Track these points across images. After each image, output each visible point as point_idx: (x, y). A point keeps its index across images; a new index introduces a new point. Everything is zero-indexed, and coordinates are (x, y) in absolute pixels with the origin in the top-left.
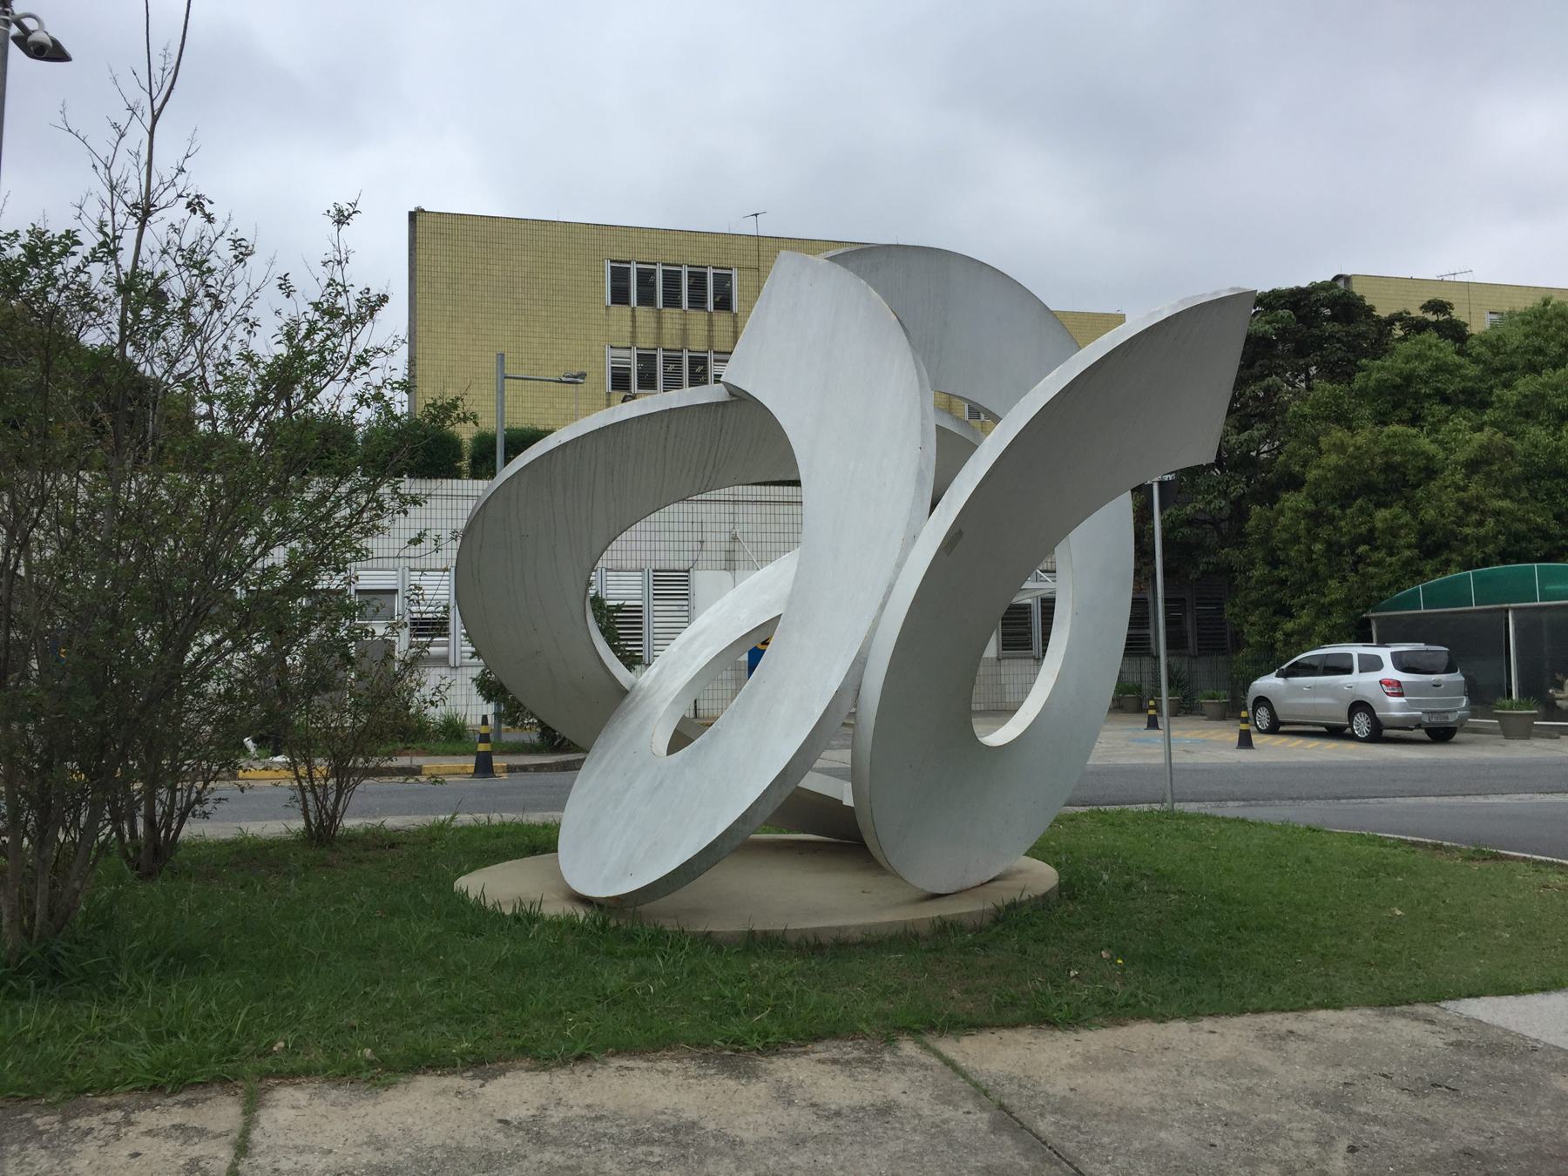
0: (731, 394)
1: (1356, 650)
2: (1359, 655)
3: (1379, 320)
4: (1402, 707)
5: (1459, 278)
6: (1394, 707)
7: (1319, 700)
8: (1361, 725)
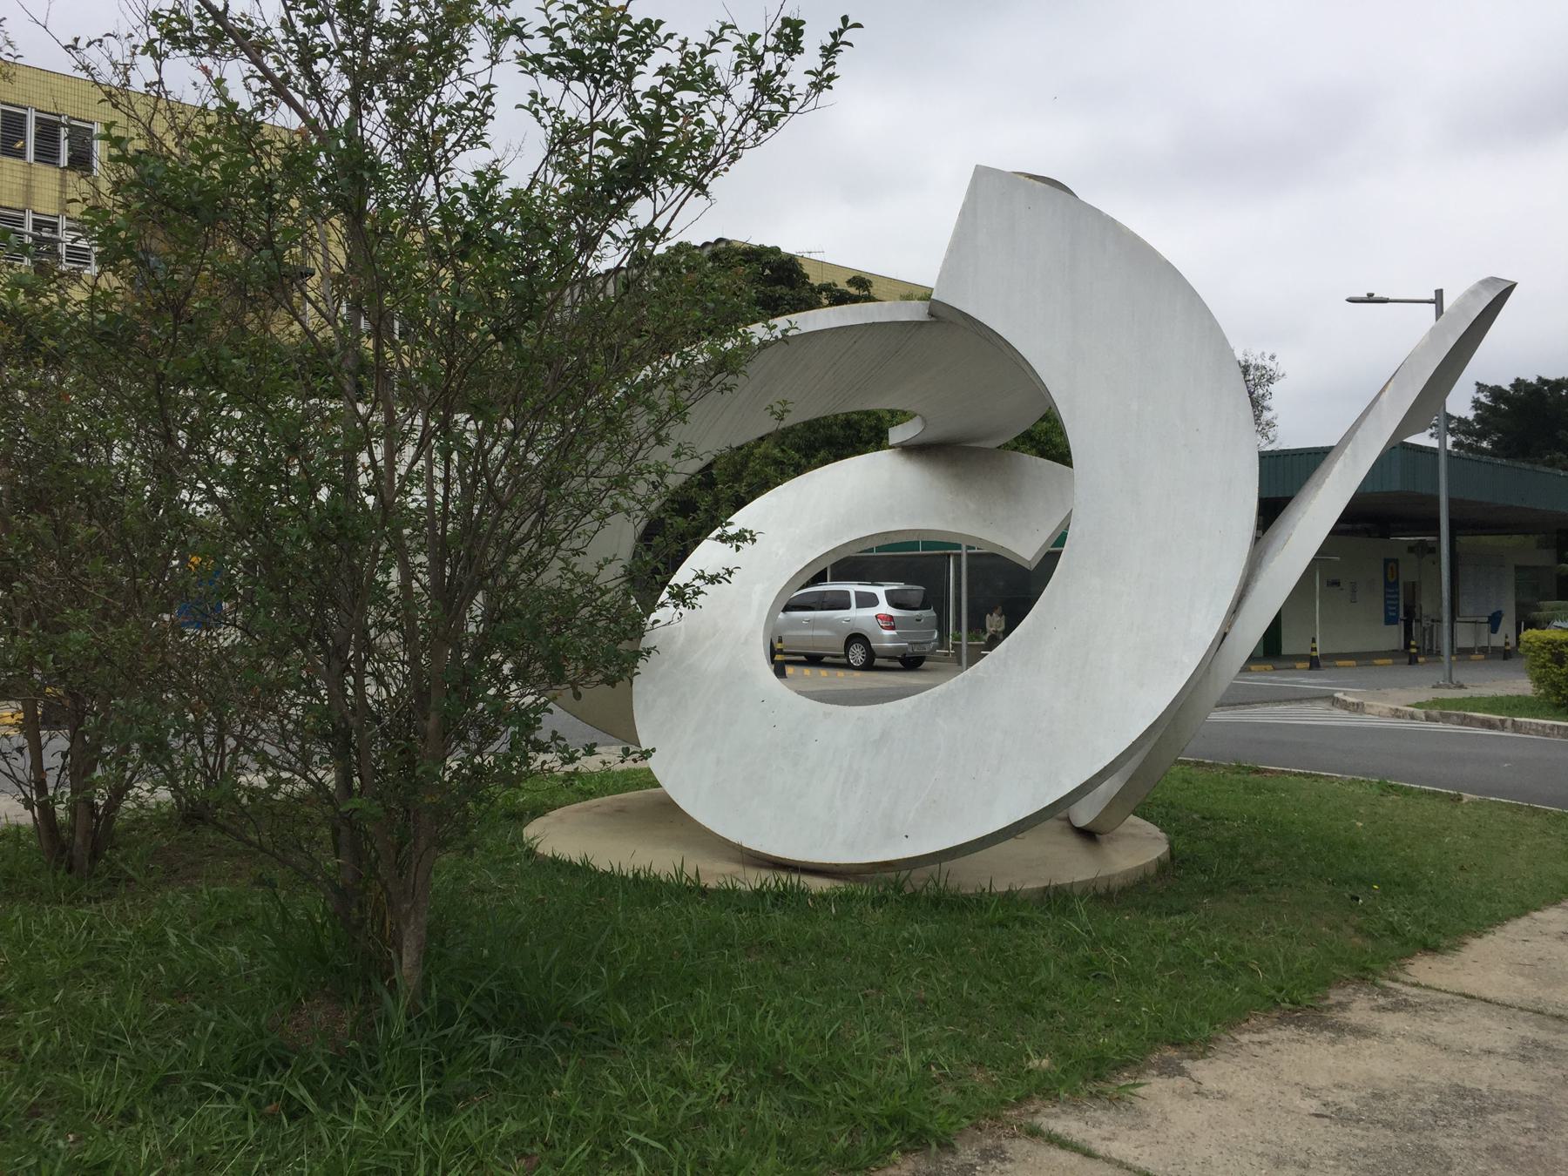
0: (931, 314)
1: (853, 588)
2: (857, 593)
3: (812, 288)
4: (893, 639)
5: (813, 256)
6: (886, 639)
7: (817, 633)
8: (857, 655)
